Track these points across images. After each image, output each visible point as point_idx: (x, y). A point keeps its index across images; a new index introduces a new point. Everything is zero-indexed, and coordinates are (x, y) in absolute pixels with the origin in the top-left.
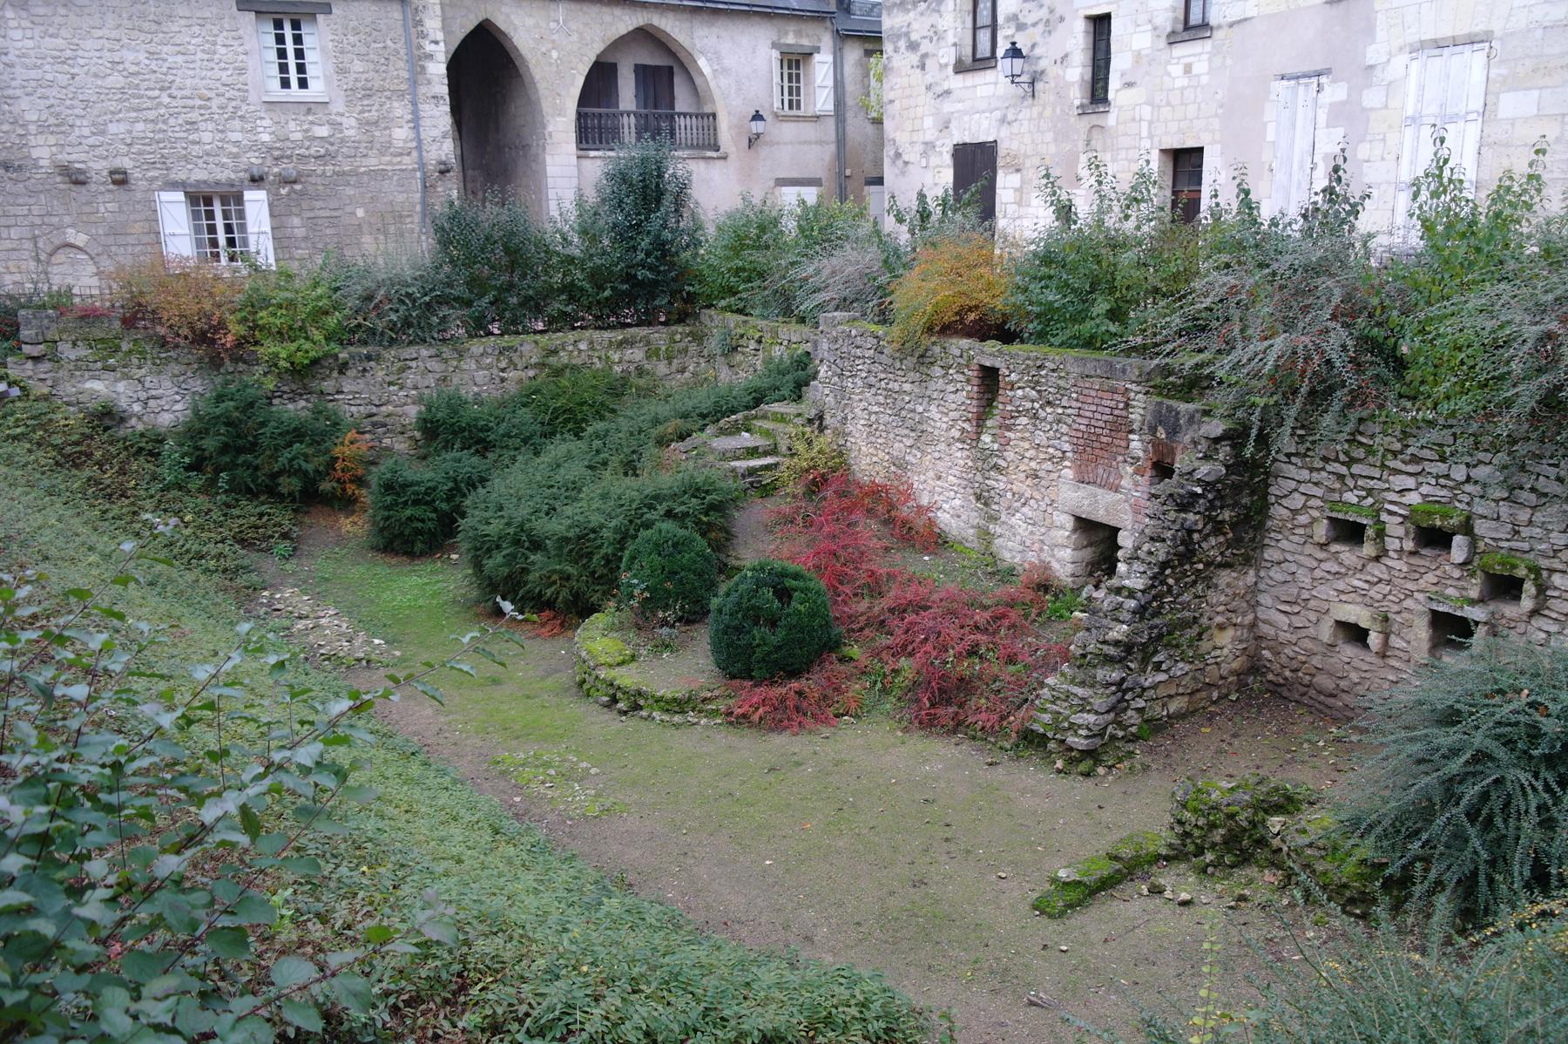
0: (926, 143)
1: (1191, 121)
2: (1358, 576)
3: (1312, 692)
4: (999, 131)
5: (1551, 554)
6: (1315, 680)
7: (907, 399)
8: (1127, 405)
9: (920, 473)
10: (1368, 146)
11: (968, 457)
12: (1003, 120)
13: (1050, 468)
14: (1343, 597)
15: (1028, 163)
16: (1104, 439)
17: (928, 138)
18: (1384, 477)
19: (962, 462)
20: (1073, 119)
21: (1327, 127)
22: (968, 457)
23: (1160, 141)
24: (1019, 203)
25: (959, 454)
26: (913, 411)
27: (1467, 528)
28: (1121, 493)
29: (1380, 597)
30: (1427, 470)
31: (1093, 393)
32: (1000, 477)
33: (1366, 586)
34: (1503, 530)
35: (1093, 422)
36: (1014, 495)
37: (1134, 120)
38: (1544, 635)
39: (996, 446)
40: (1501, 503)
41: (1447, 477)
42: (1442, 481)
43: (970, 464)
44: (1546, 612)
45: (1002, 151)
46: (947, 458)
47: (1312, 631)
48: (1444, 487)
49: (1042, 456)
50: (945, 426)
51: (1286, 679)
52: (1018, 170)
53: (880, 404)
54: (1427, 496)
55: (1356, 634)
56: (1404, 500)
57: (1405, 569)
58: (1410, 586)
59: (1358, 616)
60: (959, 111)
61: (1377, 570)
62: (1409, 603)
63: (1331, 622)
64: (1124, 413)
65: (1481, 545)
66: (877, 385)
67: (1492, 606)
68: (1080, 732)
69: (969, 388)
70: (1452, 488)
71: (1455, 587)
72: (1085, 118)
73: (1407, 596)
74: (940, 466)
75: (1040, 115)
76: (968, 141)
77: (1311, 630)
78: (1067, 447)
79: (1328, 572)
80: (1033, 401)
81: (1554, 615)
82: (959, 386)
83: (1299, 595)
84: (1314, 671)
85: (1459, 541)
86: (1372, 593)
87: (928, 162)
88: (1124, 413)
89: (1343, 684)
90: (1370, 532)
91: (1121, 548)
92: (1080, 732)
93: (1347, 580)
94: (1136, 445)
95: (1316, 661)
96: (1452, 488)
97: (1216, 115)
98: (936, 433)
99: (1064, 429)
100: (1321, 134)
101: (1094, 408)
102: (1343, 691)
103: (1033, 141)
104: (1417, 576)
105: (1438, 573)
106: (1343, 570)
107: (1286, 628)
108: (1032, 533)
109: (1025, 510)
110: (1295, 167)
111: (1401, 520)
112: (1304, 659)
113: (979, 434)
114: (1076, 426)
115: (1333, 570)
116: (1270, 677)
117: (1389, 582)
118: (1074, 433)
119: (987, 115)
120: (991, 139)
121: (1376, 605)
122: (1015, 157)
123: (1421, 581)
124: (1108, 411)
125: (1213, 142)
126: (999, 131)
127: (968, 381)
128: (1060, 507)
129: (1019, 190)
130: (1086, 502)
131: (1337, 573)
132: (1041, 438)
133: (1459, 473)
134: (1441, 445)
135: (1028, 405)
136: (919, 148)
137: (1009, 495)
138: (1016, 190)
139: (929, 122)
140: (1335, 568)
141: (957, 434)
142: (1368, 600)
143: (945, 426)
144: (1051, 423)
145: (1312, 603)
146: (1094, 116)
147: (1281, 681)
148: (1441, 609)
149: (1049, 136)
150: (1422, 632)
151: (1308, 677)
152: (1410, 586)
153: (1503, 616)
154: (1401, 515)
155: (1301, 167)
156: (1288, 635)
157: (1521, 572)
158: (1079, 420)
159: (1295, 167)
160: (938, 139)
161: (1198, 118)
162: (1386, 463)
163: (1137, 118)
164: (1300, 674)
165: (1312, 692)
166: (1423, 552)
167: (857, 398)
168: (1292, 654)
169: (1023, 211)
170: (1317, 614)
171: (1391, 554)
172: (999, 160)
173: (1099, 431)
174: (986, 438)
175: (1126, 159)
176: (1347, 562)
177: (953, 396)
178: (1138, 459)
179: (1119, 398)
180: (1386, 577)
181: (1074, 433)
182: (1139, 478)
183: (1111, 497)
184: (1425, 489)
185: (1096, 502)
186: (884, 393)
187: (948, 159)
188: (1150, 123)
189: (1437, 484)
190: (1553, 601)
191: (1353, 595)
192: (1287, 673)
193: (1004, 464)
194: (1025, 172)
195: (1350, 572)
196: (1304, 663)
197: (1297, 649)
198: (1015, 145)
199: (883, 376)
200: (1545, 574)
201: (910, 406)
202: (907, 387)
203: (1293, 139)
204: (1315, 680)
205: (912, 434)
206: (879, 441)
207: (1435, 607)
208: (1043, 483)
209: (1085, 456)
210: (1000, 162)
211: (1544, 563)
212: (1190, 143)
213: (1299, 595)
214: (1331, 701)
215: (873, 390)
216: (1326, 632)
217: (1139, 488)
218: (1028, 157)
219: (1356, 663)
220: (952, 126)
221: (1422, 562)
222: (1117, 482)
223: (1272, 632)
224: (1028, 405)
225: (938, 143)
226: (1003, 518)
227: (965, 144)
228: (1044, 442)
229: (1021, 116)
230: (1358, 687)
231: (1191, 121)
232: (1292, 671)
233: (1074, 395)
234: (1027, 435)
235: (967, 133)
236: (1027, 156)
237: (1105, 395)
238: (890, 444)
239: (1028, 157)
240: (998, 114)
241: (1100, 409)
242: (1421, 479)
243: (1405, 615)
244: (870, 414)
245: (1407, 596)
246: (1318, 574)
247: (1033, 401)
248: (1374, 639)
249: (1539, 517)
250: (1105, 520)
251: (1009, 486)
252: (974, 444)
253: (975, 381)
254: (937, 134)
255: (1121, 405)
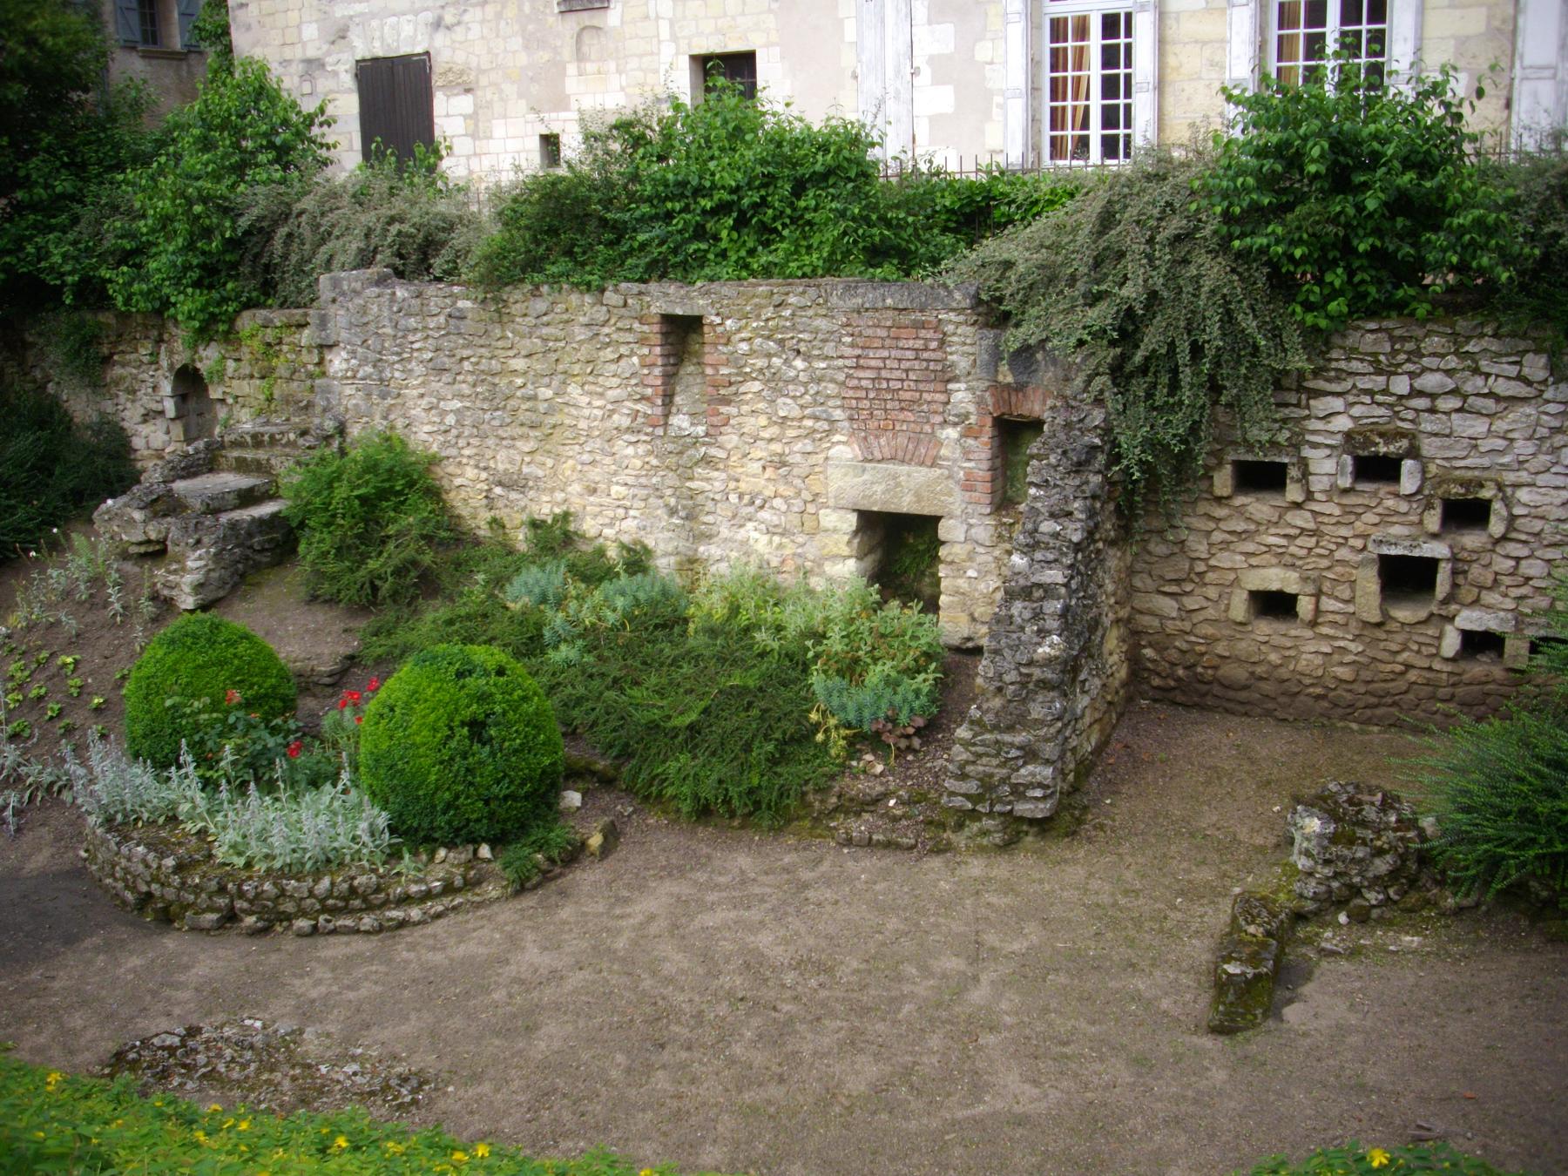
0: (309, 62)
1: (733, 18)
2: (1273, 530)
3: (1216, 689)
4: (431, 38)
5: (1516, 466)
6: (1220, 672)
7: (519, 381)
8: (942, 343)
9: (552, 490)
10: (990, 44)
11: (649, 453)
12: (438, 24)
13: (809, 448)
14: (1253, 561)
15: (484, 81)
16: (907, 395)
17: (311, 53)
18: (1304, 402)
19: (639, 463)
20: (551, 20)
21: (930, 23)
22: (649, 453)
23: (689, 45)
24: (474, 136)
25: (630, 451)
26: (531, 398)
27: (1413, 453)
28: (941, 467)
29: (1303, 552)
30: (1360, 386)
31: (882, 333)
32: (716, 474)
33: (1283, 542)
34: (1458, 446)
35: (884, 374)
36: (741, 497)
37: (647, 17)
38: (1512, 563)
39: (701, 430)
40: (1454, 416)
41: (1385, 392)
42: (1379, 398)
43: (655, 462)
44: (1514, 535)
45: (439, 64)
46: (608, 460)
47: (1211, 613)
48: (1379, 404)
49: (791, 433)
50: (599, 413)
51: (1178, 680)
52: (468, 91)
53: (462, 396)
54: (1360, 418)
55: (1275, 605)
56: (1330, 427)
57: (1337, 511)
58: (1344, 531)
59: (1282, 580)
60: (362, 14)
61: (1301, 519)
62: (1342, 554)
63: (1245, 595)
64: (938, 355)
65: (1433, 469)
66: (456, 368)
67: (1449, 538)
68: (1030, 793)
69: (645, 351)
70: (1390, 406)
71: (1401, 524)
72: (573, 16)
73: (1339, 545)
74: (595, 474)
75: (499, 16)
76: (380, 54)
77: (1211, 611)
78: (838, 414)
79: (1230, 533)
80: (769, 356)
81: (1523, 537)
82: (623, 350)
83: (1191, 568)
84: (1216, 661)
85: (1408, 465)
86: (1293, 549)
87: (313, 87)
88: (938, 355)
89: (1259, 670)
90: (1294, 472)
91: (943, 543)
92: (1030, 793)
93: (1258, 539)
94: (962, 396)
95: (1221, 649)
96: (1390, 406)
97: (770, 10)
98: (583, 424)
99: (831, 389)
100: (921, 32)
101: (885, 353)
102: (1261, 679)
103: (490, 51)
104: (1352, 518)
105: (1379, 510)
106: (1253, 527)
107: (1174, 614)
108: (780, 546)
109: (764, 515)
110: (890, 73)
111: (1328, 452)
112: (1203, 649)
113: (667, 415)
114: (854, 383)
115: (1239, 529)
116: (1156, 681)
117: (1313, 533)
118: (851, 393)
119: (410, 17)
120: (419, 50)
121: (1299, 563)
122: (462, 73)
123: (1358, 524)
124: (910, 355)
125: (768, 45)
126: (431, 38)
127: (642, 341)
128: (831, 502)
129: (473, 117)
130: (879, 488)
131: (1245, 532)
132: (786, 407)
133: (1401, 385)
134: (1375, 354)
135: (760, 363)
136: (297, 68)
137: (733, 498)
138: (466, 117)
139: (310, 32)
140: (1241, 526)
141: (626, 422)
142: (1289, 560)
143: (599, 413)
144: (805, 384)
145: (1210, 577)
146: (585, 15)
147: (1172, 683)
148: (1393, 551)
149: (516, 43)
150: (1369, 582)
151: (1210, 672)
152: (1344, 531)
153: (1463, 549)
154: (1327, 446)
155: (898, 72)
156: (1178, 623)
157: (1486, 494)
158: (861, 374)
159: (890, 73)
160: (329, 53)
161: (743, 14)
162: (1305, 384)
163: (652, 15)
164: (1200, 670)
165: (1216, 689)
166: (1360, 487)
167: (415, 393)
168: (1185, 646)
169: (482, 145)
170: (1219, 589)
171: (1318, 496)
172: (434, 78)
173: (896, 385)
174: (680, 421)
175: (640, 69)
176: (1258, 516)
177: (613, 367)
178: (967, 416)
179: (930, 334)
180: (1311, 526)
181: (851, 393)
182: (970, 441)
183: (921, 475)
184: (1357, 411)
185: (898, 485)
186: (470, 379)
187: (348, 80)
188: (672, 23)
189: (1373, 402)
190: (1522, 520)
191: (1267, 556)
192: (1181, 672)
193: (722, 454)
194: (479, 93)
195: (1262, 528)
196: (1203, 654)
197: (1193, 639)
198: (460, 58)
199: (466, 353)
200: (1509, 491)
201: (529, 390)
202: (519, 364)
203: (883, 39)
204: (1220, 672)
205: (533, 433)
206: (467, 452)
207: (1385, 550)
208: (796, 471)
209: (872, 424)
210: (437, 81)
211: (1510, 477)
212: (735, 46)
213: (1191, 568)
214: (1243, 695)
215: (446, 378)
216: (1239, 607)
217: (975, 456)
218: (485, 71)
219: (1276, 640)
220: (352, 36)
221: (1360, 501)
222: (933, 452)
223: (1156, 623)
224: (760, 363)
225: (329, 60)
226: (725, 532)
227: (375, 60)
228: (797, 413)
229: (467, 17)
230: (1282, 670)
231: (733, 18)
232: (1186, 668)
233: (848, 339)
234: (762, 405)
235: (377, 44)
236: (481, 71)
237: (904, 333)
238: (489, 454)
239: (485, 71)
240: (429, 16)
241: (894, 353)
242: (1351, 399)
243: (1339, 569)
244: (443, 413)
245: (1339, 545)
246: (1217, 537)
247: (769, 356)
248: (1305, 606)
249: (1500, 425)
250: (915, 509)
251: (732, 485)
252: (660, 431)
253: (657, 339)
254: (325, 47)
255: (934, 345)
